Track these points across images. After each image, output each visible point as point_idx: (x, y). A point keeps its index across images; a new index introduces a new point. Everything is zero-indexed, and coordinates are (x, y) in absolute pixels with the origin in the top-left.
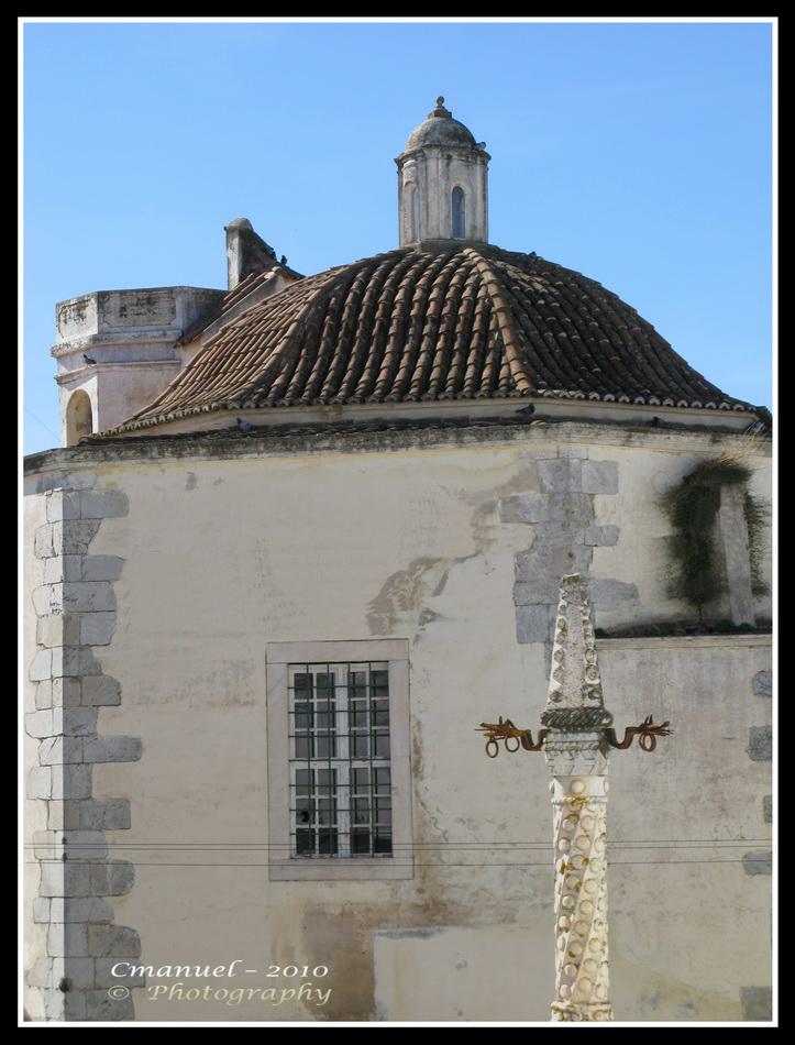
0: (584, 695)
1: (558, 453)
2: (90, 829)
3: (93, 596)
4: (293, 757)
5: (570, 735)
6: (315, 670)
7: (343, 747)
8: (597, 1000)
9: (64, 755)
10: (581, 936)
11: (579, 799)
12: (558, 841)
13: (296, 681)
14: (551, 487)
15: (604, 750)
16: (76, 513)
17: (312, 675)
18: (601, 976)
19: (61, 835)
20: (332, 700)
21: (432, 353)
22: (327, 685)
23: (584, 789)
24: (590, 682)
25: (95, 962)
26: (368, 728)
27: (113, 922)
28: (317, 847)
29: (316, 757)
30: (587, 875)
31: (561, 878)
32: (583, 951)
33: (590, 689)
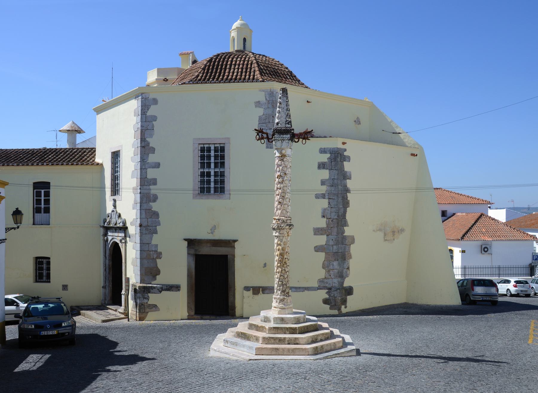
0: (286, 124)
1: (270, 90)
2: (146, 186)
4: (200, 168)
5: (281, 135)
6: (206, 146)
7: (212, 165)
8: (287, 216)
9: (140, 167)
10: (283, 197)
11: (284, 155)
12: (277, 168)
14: (268, 99)
16: (144, 104)
17: (205, 147)
18: (289, 209)
19: (139, 187)
20: (210, 154)
21: (238, 72)
23: (285, 152)
24: (288, 120)
25: (148, 220)
26: (219, 161)
27: (152, 210)
29: (205, 168)
30: (285, 178)
31: (278, 104)
32: (284, 201)
33: (288, 122)
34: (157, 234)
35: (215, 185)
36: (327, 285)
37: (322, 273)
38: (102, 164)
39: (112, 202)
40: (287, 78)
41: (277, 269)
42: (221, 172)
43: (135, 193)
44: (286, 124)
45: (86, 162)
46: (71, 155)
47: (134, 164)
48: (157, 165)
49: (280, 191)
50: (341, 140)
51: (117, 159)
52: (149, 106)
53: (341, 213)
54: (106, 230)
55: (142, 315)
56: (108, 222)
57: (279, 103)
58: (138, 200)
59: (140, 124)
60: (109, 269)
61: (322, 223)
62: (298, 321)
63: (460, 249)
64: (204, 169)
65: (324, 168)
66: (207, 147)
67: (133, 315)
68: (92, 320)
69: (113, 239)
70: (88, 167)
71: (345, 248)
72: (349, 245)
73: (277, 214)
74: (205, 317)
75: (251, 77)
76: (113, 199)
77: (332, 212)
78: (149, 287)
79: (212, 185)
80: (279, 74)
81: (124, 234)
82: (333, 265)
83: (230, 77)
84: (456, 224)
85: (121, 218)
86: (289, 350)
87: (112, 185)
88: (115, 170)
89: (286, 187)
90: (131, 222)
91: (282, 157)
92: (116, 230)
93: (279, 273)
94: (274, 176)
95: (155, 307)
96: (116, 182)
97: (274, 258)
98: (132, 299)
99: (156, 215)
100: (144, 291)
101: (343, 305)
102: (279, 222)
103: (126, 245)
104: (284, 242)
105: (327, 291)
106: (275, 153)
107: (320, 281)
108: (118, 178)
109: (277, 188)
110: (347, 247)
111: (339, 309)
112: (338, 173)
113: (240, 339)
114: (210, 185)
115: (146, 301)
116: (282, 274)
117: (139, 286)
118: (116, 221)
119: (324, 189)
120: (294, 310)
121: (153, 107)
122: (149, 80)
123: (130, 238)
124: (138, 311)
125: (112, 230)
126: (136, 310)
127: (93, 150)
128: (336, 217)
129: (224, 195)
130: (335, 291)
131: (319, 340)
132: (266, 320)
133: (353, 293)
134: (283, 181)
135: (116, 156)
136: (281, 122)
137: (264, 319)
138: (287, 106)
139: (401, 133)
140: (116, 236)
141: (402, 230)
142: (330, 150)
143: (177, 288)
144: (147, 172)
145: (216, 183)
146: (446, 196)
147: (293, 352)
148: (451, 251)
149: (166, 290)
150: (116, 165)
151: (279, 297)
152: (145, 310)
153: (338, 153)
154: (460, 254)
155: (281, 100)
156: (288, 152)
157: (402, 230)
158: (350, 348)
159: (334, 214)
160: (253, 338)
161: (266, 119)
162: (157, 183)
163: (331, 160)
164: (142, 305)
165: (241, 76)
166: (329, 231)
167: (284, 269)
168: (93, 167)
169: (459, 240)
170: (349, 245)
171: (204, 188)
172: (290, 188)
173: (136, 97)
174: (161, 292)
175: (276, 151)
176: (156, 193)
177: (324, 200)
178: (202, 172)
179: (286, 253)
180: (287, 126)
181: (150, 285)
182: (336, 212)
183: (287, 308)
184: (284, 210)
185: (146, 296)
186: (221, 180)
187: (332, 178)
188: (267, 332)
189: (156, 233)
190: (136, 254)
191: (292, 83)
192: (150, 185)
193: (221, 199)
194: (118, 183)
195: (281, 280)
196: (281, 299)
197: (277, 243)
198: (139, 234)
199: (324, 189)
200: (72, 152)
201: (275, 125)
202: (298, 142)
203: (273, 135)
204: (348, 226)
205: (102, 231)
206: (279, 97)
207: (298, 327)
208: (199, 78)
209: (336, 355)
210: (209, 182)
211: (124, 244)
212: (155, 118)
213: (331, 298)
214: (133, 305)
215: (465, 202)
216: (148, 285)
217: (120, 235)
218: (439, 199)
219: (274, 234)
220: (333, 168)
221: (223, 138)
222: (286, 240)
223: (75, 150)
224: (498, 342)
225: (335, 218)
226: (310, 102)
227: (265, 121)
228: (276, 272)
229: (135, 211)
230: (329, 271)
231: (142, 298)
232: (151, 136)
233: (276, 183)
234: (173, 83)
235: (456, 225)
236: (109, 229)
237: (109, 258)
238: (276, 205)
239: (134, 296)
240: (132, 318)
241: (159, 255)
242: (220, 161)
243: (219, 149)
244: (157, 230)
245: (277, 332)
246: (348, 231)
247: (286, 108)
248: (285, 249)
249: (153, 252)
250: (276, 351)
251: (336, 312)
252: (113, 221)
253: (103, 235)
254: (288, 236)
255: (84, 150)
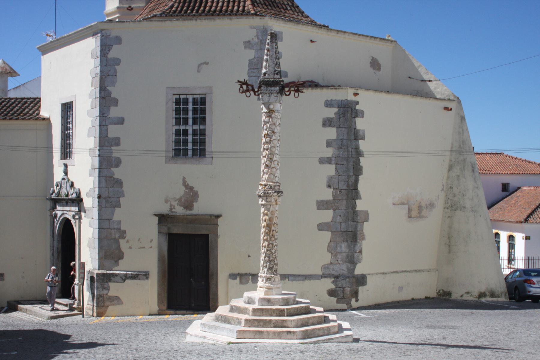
0: (274, 74)
1: (264, 27)
2: (107, 147)
3: (110, 71)
4: (174, 124)
5: (269, 88)
6: (182, 97)
7: (190, 121)
9: (99, 123)
10: (271, 159)
11: (272, 111)
12: (263, 126)
13: (175, 131)
15: (281, 94)
18: (277, 173)
19: (98, 148)
20: (187, 107)
22: (183, 155)
24: (276, 69)
26: (198, 147)
27: (114, 177)
28: (181, 155)
30: (274, 138)
31: (266, 51)
33: (277, 72)
34: (120, 207)
35: (194, 146)
36: (333, 273)
37: (327, 258)
38: (49, 119)
39: (63, 168)
40: (287, 9)
41: (264, 242)
42: (201, 130)
43: (92, 155)
44: (274, 74)
45: (28, 116)
46: (8, 107)
47: (91, 119)
48: (121, 121)
49: (267, 152)
50: (351, 91)
51: (68, 113)
52: (111, 47)
53: (352, 182)
54: (54, 203)
55: (101, 310)
56: (57, 193)
57: (267, 49)
58: (97, 165)
59: (99, 68)
60: (58, 253)
61: (328, 195)
62: (286, 302)
63: (524, 235)
64: (179, 126)
65: (330, 125)
66: (183, 98)
67: (89, 309)
68: (37, 316)
69: (63, 214)
70: (31, 122)
71: (356, 227)
72: (362, 222)
73: (263, 179)
74: (177, 312)
75: (241, 8)
76: (64, 164)
77: (340, 181)
78: (110, 274)
79: (190, 146)
80: (276, 3)
81: (78, 208)
82: (341, 247)
83: (213, 8)
84: (520, 201)
85: (74, 188)
86: (274, 333)
87: (62, 146)
88: (66, 126)
89: (274, 148)
90: (87, 193)
91: (270, 113)
92: (67, 203)
93: (265, 248)
94: (261, 135)
95: (116, 300)
96: (68, 142)
97: (260, 231)
98: (88, 291)
99: (119, 183)
100: (103, 280)
101: (353, 298)
102: (265, 189)
103: (80, 223)
104: (272, 211)
105: (333, 279)
106: (262, 108)
107: (325, 268)
108: (69, 137)
109: (264, 149)
110: (359, 225)
111: (349, 303)
112: (348, 132)
113: (220, 323)
114: (187, 146)
115: (105, 292)
116: (269, 249)
117: (97, 274)
118: (68, 192)
119: (329, 152)
120: (283, 292)
121: (115, 47)
122: (108, 9)
123: (85, 212)
124: (95, 305)
125: (61, 204)
126: (93, 304)
127: (37, 100)
128: (345, 187)
129: (205, 159)
130: (343, 280)
131: (311, 324)
132: (250, 301)
133: (366, 283)
134: (271, 140)
135: (68, 109)
136: (268, 73)
137: (248, 301)
138: (276, 53)
139: (432, 81)
140: (67, 211)
141: (431, 205)
142: (338, 103)
143: (146, 275)
144: (107, 129)
145: (195, 144)
146: (509, 164)
147: (279, 335)
148: (497, 235)
149: (131, 278)
150: (67, 120)
151: (265, 275)
152: (104, 303)
153: (348, 107)
154: (523, 241)
155: (269, 47)
156: (277, 107)
157: (431, 205)
158: (346, 333)
159: (343, 183)
160: (234, 321)
161: (258, 63)
162: (120, 144)
163: (339, 116)
164: (101, 296)
165: (228, 6)
166: (336, 204)
167: (271, 242)
168: (38, 122)
169: (522, 222)
170: (362, 222)
171: (180, 149)
172: (278, 149)
173: (94, 34)
174: (124, 280)
175: (262, 106)
176: (118, 156)
177: (331, 165)
178: (177, 129)
179: (274, 224)
180: (276, 76)
181: (111, 272)
182: (345, 181)
183: (275, 288)
184: (272, 174)
185: (105, 286)
186: (201, 139)
187: (341, 138)
188: (251, 314)
189: (119, 206)
190: (93, 233)
191: (294, 15)
192: (111, 146)
193: (201, 164)
194: (70, 143)
195: (268, 256)
196: (267, 277)
197: (264, 213)
198: (98, 207)
199: (329, 152)
200: (9, 103)
201: (262, 76)
202: (289, 95)
203: (260, 87)
204: (360, 198)
205: (49, 204)
206: (267, 43)
207: (286, 309)
208: (174, 9)
209: (329, 341)
210: (186, 142)
211: (77, 221)
212: (117, 62)
213: (338, 288)
214: (89, 297)
215: (536, 172)
216: (109, 272)
217: (73, 209)
218: (499, 168)
219: (260, 202)
220: (341, 126)
221: (203, 87)
222: (274, 209)
223: (13, 101)
224: (532, 336)
225: (343, 188)
226: (314, 42)
227: (256, 65)
228: (262, 247)
229: (92, 179)
230: (336, 255)
231: (101, 288)
232: (113, 84)
233: (262, 143)
234: (140, 15)
235: (520, 203)
236: (58, 202)
237: (57, 239)
238: (262, 168)
239: (90, 286)
240: (88, 314)
241: (123, 234)
242: (201, 116)
243: (199, 101)
244: (120, 203)
245: (262, 314)
246: (360, 205)
247: (274, 56)
248: (273, 219)
249: (115, 230)
250: (260, 335)
251: (344, 306)
252: (64, 192)
253: (50, 209)
254: (276, 204)
255: (25, 100)
